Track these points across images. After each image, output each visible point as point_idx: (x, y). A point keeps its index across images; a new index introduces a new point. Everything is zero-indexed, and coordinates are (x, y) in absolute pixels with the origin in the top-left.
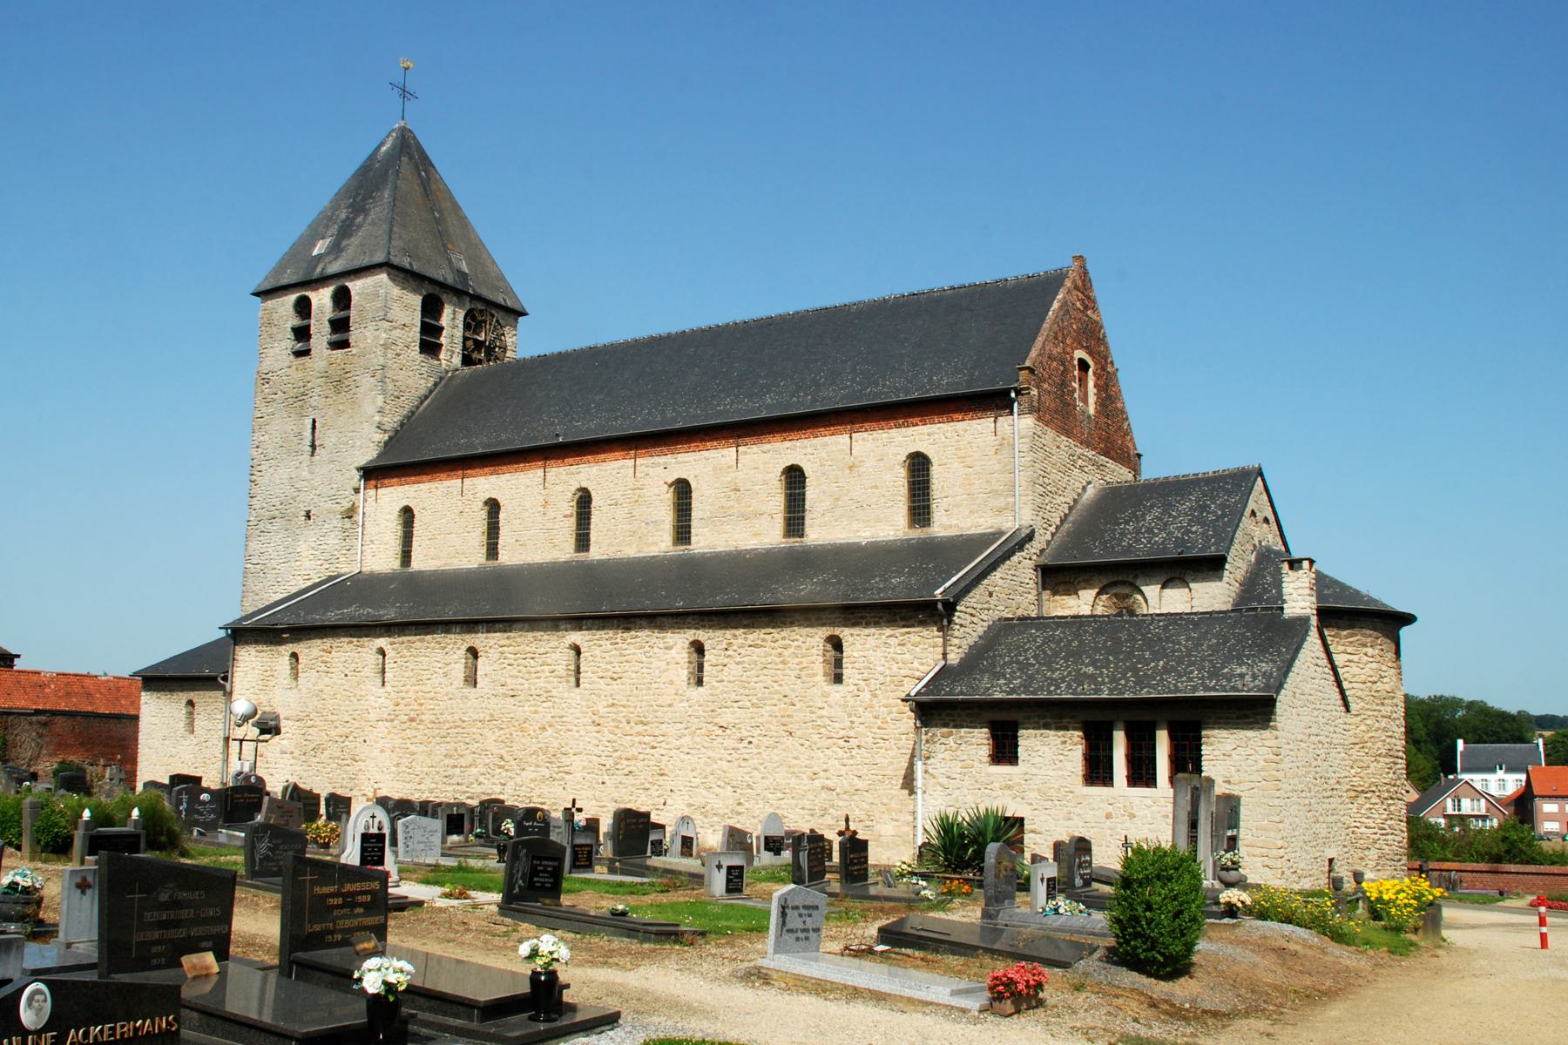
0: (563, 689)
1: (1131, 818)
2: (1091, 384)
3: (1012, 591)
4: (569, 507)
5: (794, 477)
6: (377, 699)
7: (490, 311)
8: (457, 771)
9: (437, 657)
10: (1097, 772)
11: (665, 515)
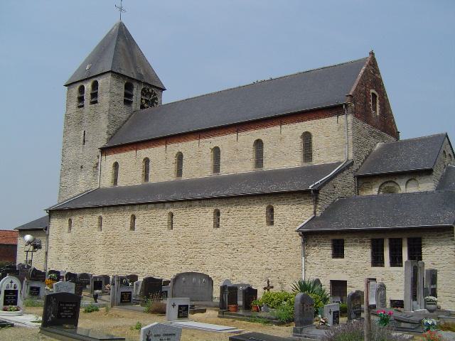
0: (165, 230)
1: (395, 280)
2: (378, 106)
4: (173, 159)
5: (259, 144)
6: (99, 235)
7: (152, 90)
8: (127, 264)
9: (119, 220)
10: (377, 261)
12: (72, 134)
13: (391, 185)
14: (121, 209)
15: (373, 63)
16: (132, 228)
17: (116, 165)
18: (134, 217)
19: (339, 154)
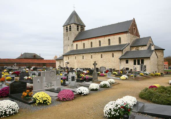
0: (90, 59)
1: (138, 67)
3: (128, 49)
5: (109, 40)
6: (75, 60)
7: (83, 26)
10: (135, 64)
11: (98, 44)
12: (66, 38)
13: (138, 48)
14: (80, 55)
15: (134, 20)
16: (83, 58)
17: (77, 45)
18: (83, 56)
19: (127, 42)
